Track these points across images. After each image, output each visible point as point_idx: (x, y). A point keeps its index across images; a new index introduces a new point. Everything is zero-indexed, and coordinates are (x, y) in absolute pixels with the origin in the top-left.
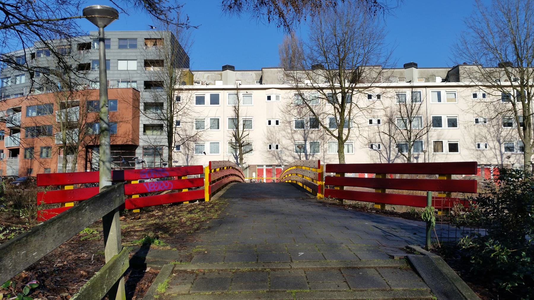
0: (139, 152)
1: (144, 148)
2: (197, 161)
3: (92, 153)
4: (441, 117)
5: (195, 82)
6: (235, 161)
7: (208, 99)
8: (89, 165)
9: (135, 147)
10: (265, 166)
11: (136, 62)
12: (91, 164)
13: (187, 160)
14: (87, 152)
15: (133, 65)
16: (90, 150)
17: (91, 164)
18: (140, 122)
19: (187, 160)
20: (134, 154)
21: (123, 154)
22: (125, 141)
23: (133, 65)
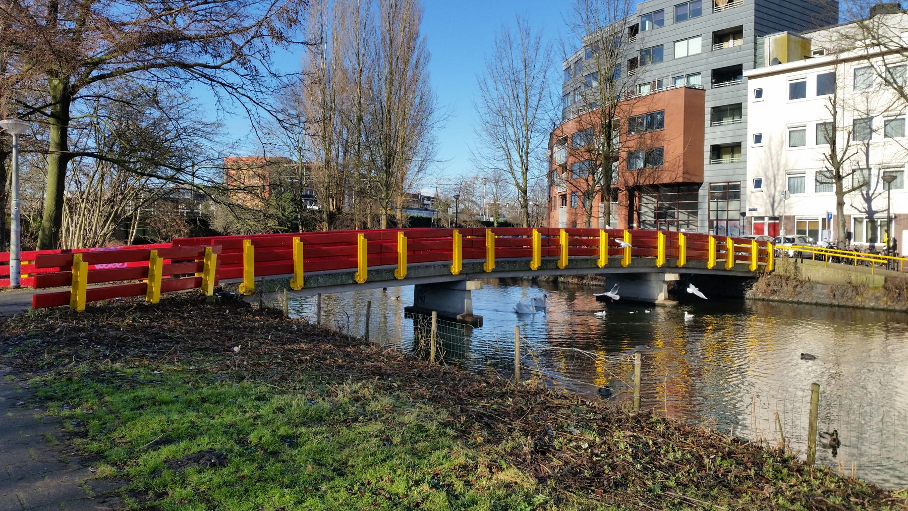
0: (703, 192)
1: (712, 188)
2: (790, 208)
3: (640, 198)
4: (804, 96)
5: (815, 53)
6: (866, 205)
7: (811, 87)
8: (635, 216)
9: (700, 184)
10: (766, 219)
11: (700, 39)
12: (639, 215)
13: (773, 206)
14: (631, 198)
15: (696, 46)
16: (636, 193)
17: (639, 215)
18: (706, 143)
19: (773, 206)
20: (696, 197)
21: (679, 198)
22: (674, 176)
23: (696, 46)
